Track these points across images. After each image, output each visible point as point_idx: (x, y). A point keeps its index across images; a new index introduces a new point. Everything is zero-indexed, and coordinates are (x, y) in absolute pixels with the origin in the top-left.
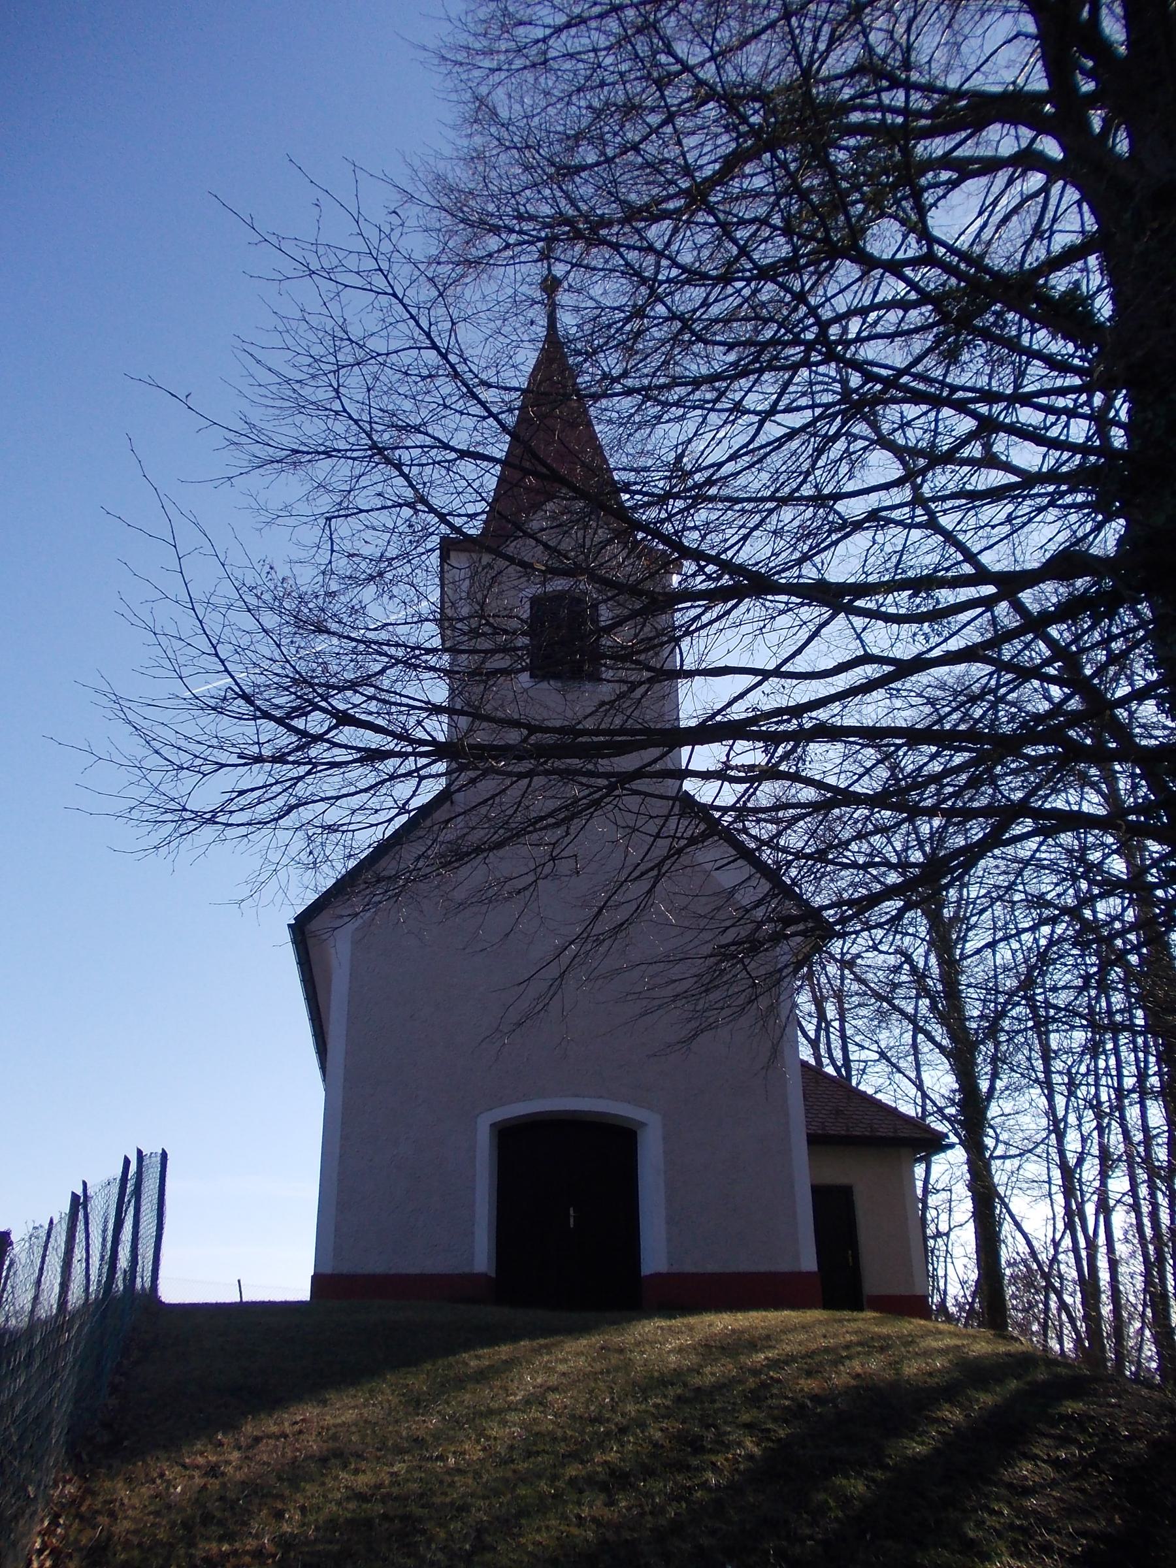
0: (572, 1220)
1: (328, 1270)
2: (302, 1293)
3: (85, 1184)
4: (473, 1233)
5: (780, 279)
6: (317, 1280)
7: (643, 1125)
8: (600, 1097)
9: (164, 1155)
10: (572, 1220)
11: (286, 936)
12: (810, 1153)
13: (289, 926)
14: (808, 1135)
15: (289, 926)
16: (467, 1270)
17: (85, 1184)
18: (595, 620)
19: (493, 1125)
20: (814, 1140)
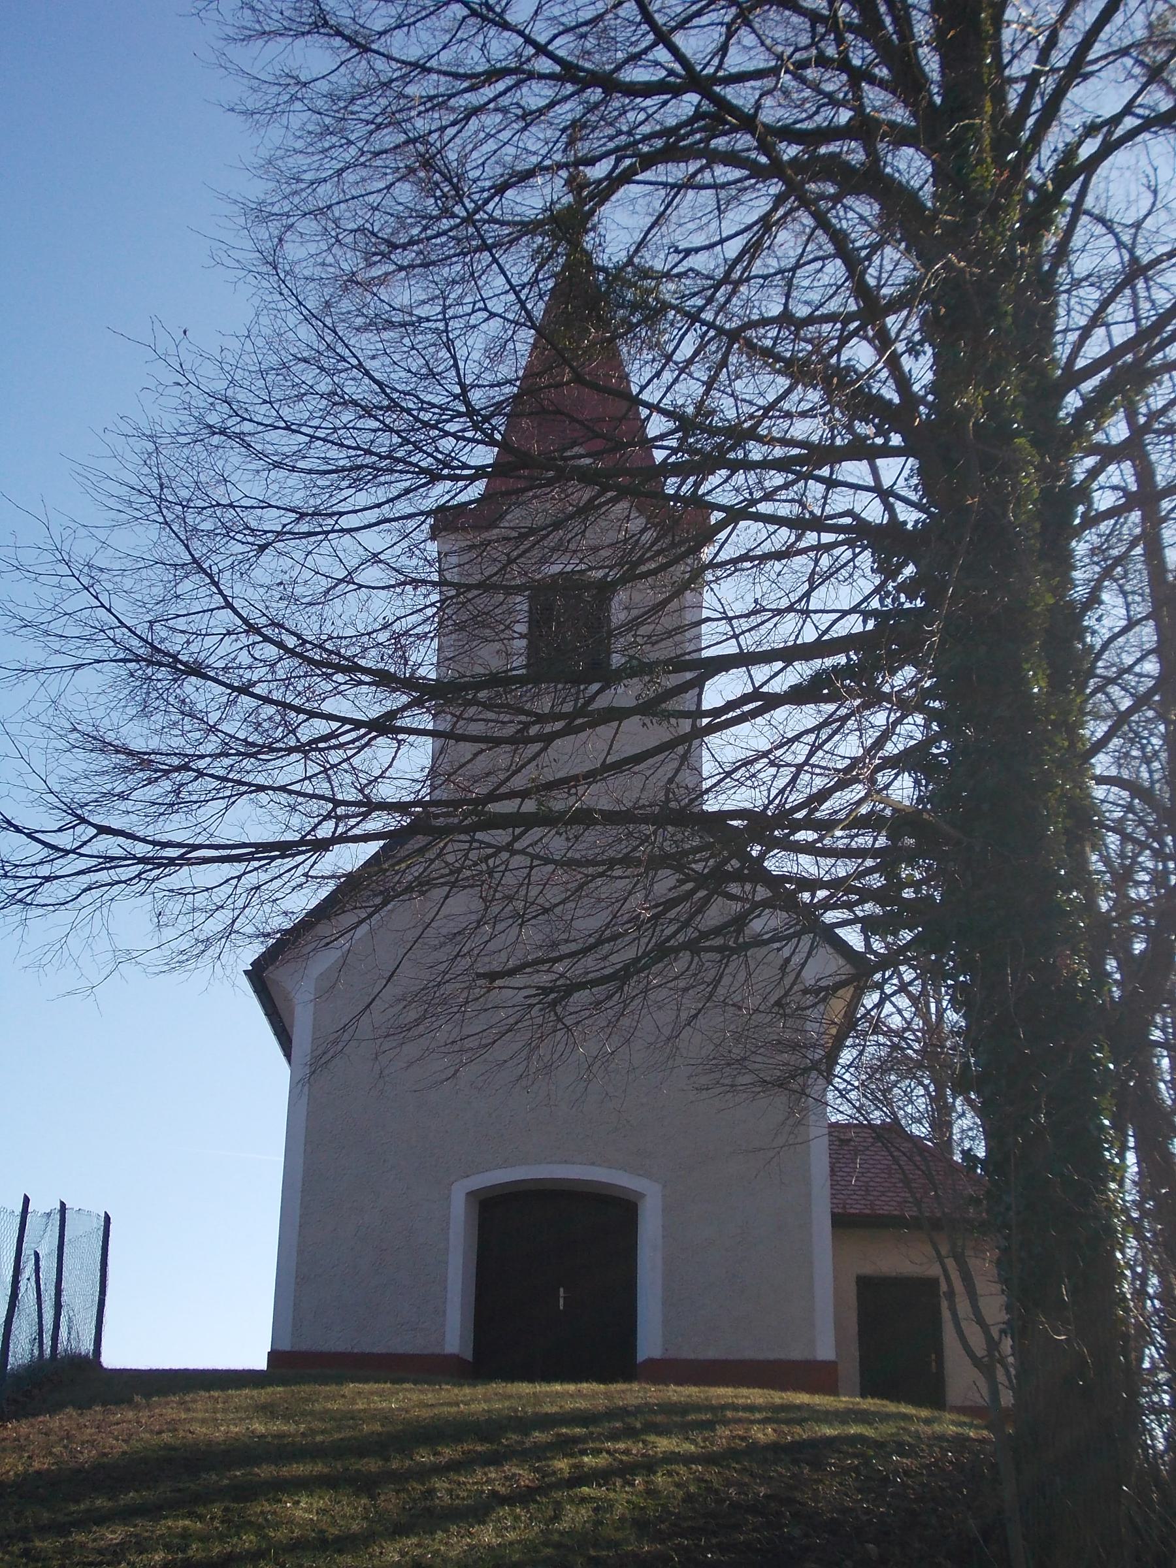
0: (562, 1301)
1: (286, 1346)
2: (261, 1364)
3: (26, 1200)
4: (444, 1312)
5: (763, 160)
6: (273, 1356)
7: (642, 1196)
8: (593, 1164)
9: (107, 1219)
10: (562, 1301)
11: (245, 984)
12: (833, 1234)
13: (246, 972)
14: (833, 1215)
15: (246, 972)
16: (437, 1350)
17: (26, 1200)
18: (1157, 1403)
19: (471, 1194)
20: (842, 1222)
